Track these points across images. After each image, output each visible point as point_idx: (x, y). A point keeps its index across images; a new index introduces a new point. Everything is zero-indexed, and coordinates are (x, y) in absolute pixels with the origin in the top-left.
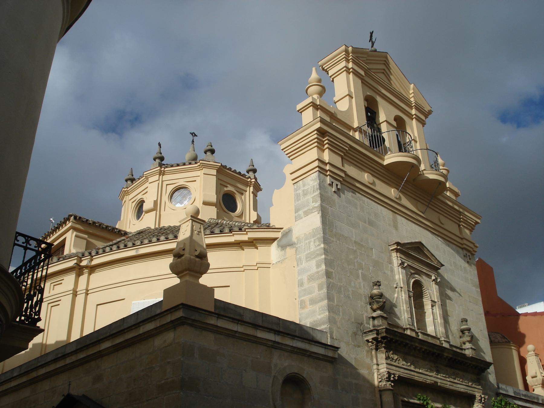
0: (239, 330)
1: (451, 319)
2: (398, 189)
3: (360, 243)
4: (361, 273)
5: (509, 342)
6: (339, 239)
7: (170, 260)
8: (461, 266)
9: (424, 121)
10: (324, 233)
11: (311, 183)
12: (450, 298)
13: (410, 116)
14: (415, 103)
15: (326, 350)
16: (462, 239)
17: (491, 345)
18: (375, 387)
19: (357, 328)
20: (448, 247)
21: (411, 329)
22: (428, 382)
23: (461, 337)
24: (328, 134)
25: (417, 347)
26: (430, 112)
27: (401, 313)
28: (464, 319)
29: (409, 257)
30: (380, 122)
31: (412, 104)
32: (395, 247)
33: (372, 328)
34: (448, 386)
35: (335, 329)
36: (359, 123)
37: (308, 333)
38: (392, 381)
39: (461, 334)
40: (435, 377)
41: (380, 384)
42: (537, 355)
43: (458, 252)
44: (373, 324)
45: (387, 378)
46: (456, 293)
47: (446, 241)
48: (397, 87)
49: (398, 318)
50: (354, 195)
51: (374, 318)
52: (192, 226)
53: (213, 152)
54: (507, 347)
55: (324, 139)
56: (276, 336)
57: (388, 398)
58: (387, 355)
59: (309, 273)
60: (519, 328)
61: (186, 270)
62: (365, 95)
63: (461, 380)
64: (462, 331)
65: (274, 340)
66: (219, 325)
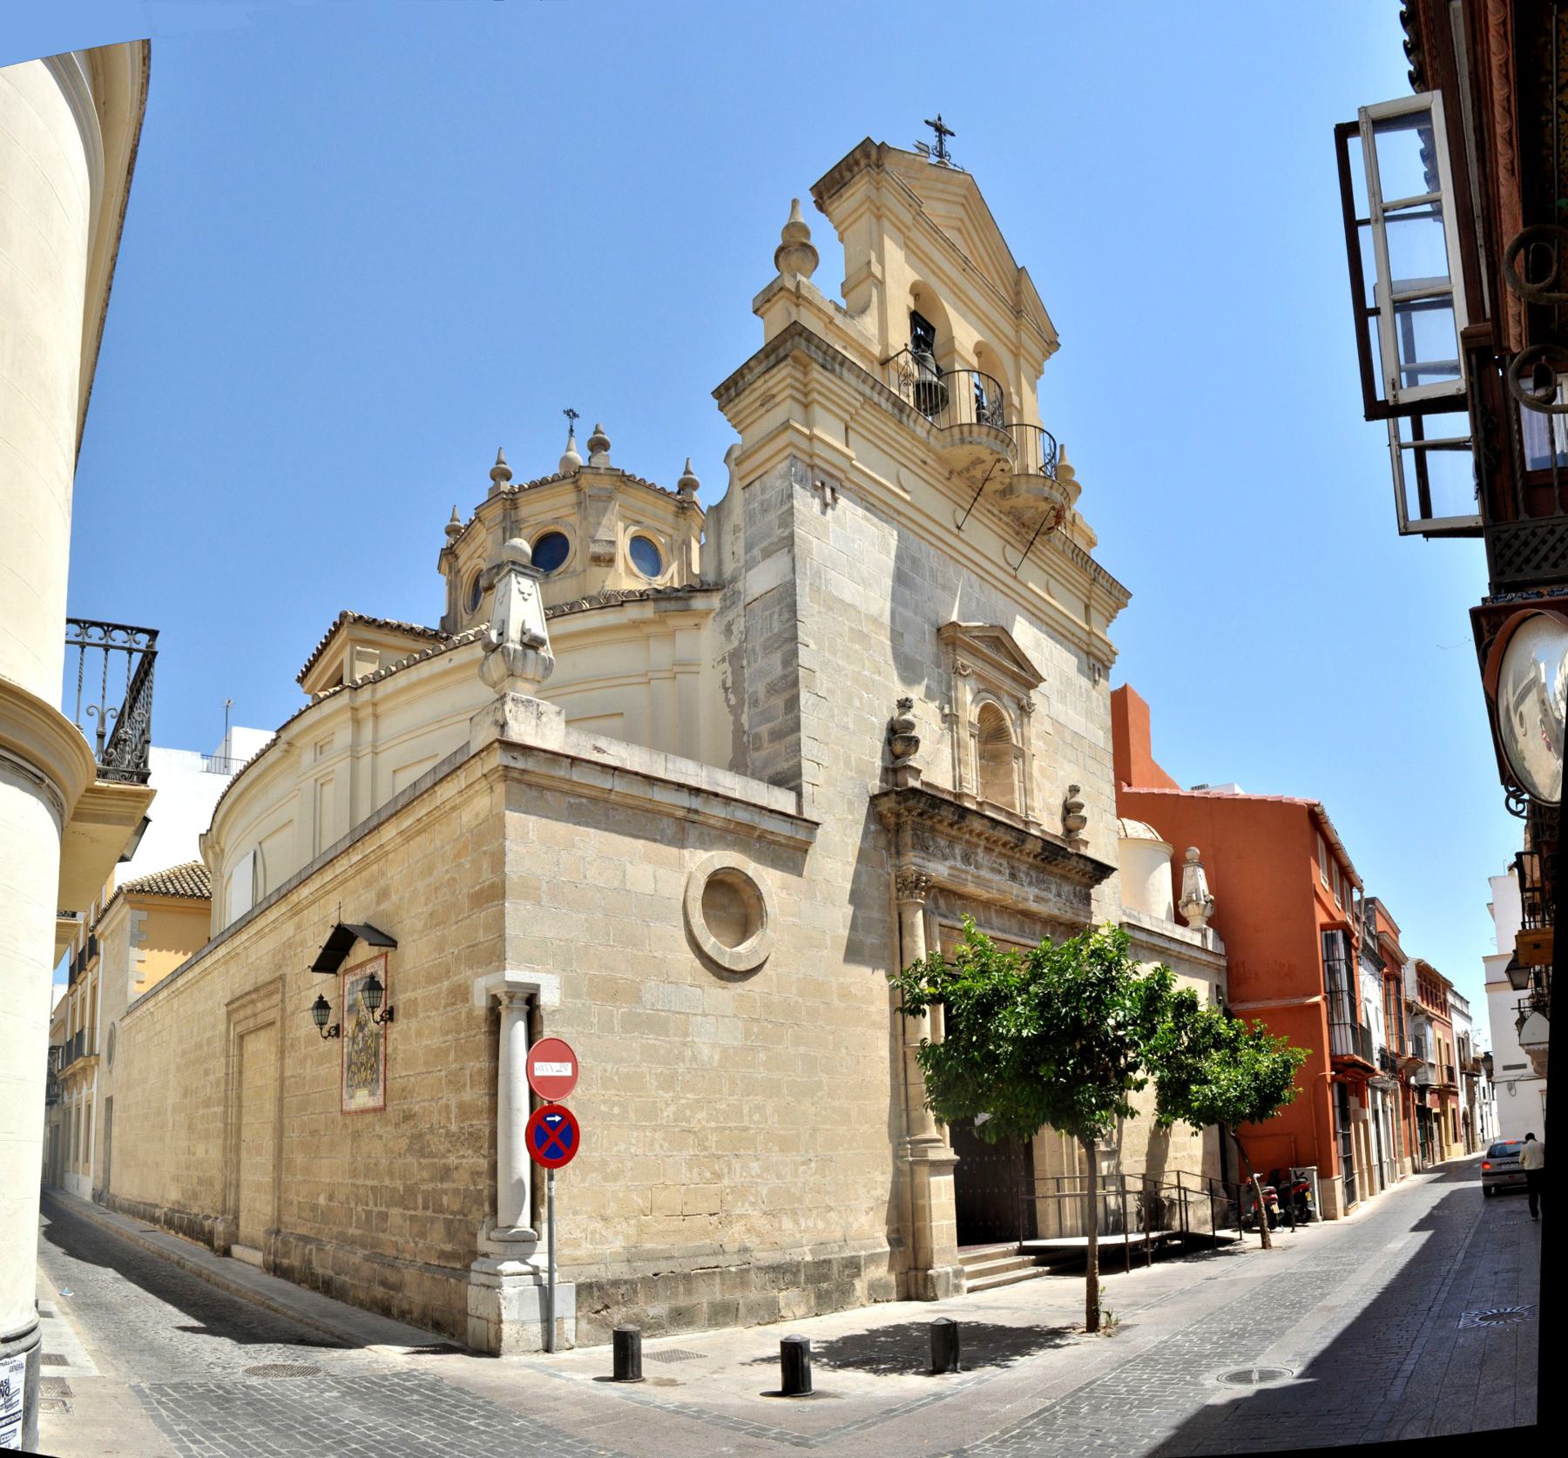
0: (617, 789)
11: (778, 483)
59: (769, 680)
65: (687, 805)
66: (575, 778)
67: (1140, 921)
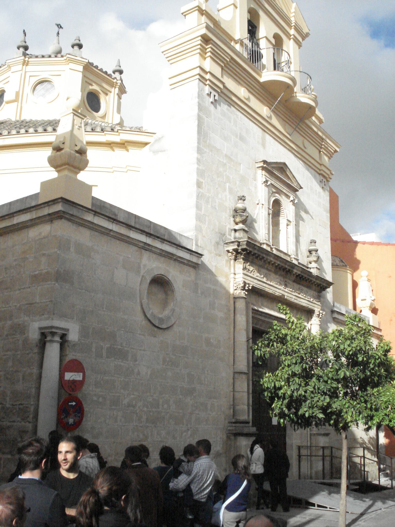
0: (114, 229)
1: (301, 239)
2: (270, 109)
3: (230, 157)
4: (229, 186)
5: (346, 266)
6: (212, 151)
7: (48, 152)
8: (316, 191)
9: (301, 43)
10: (199, 143)
12: (303, 220)
13: (288, 35)
14: (295, 23)
15: (191, 255)
16: (321, 165)
17: (332, 267)
18: (230, 294)
19: (219, 238)
20: (307, 171)
21: (267, 245)
22: (277, 294)
23: (308, 257)
24: (211, 42)
25: (271, 261)
26: (307, 35)
27: (259, 228)
28: (314, 240)
29: (272, 176)
30: (260, 37)
31: (292, 24)
32: (262, 164)
33: (233, 240)
34: (293, 300)
35: (200, 237)
36: (241, 35)
37: (176, 238)
38: (246, 291)
39: (308, 254)
40: (283, 291)
41: (235, 291)
42: (369, 280)
43: (315, 177)
44: (234, 235)
45: (242, 287)
46: (309, 215)
47: (306, 165)
48: (279, 3)
49: (257, 233)
50: (229, 108)
51: (235, 231)
52: (74, 120)
53: (80, 46)
54: (344, 270)
55: (207, 46)
56: (148, 238)
57: (241, 305)
58: (244, 266)
60: (355, 254)
61: (65, 164)
62: (249, 7)
63: (304, 295)
64: (310, 252)
65: (145, 241)
67: (340, 310)
